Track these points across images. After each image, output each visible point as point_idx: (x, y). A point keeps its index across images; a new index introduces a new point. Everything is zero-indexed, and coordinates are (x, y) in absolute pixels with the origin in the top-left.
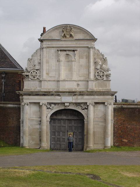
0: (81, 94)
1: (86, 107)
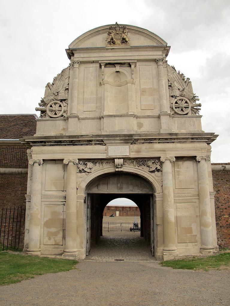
0: (149, 140)
1: (159, 168)
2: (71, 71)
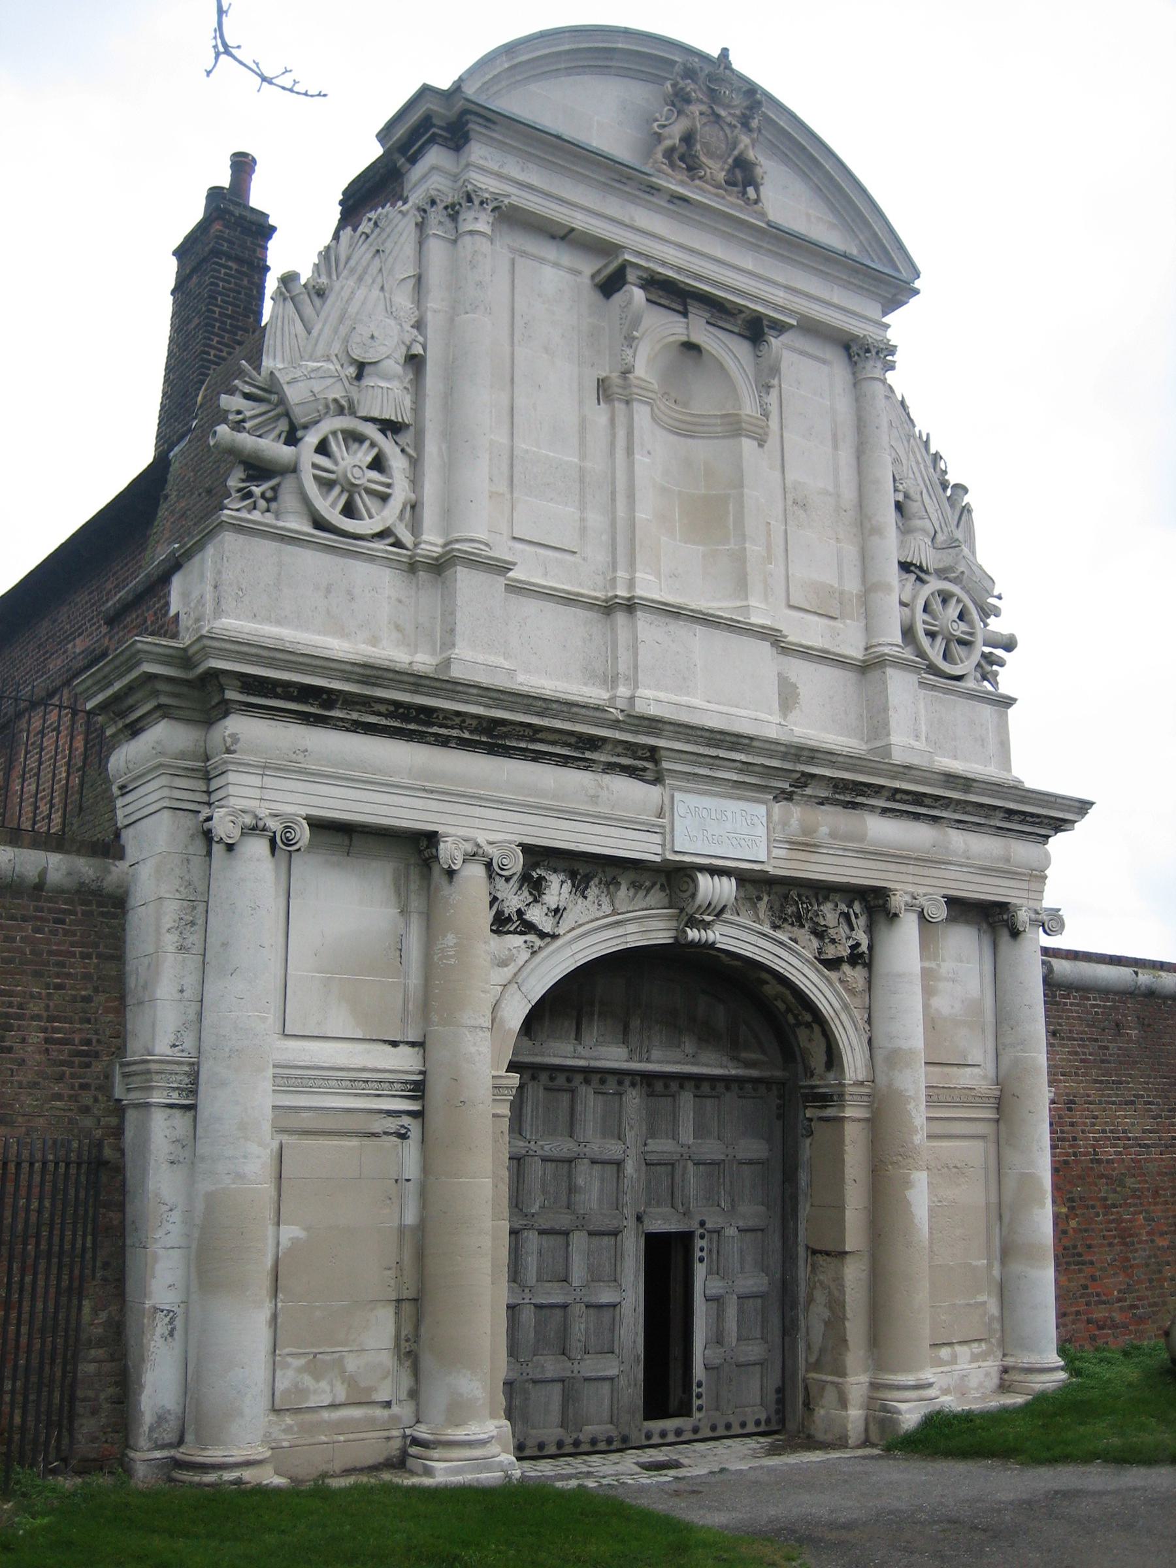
2: (436, 249)
